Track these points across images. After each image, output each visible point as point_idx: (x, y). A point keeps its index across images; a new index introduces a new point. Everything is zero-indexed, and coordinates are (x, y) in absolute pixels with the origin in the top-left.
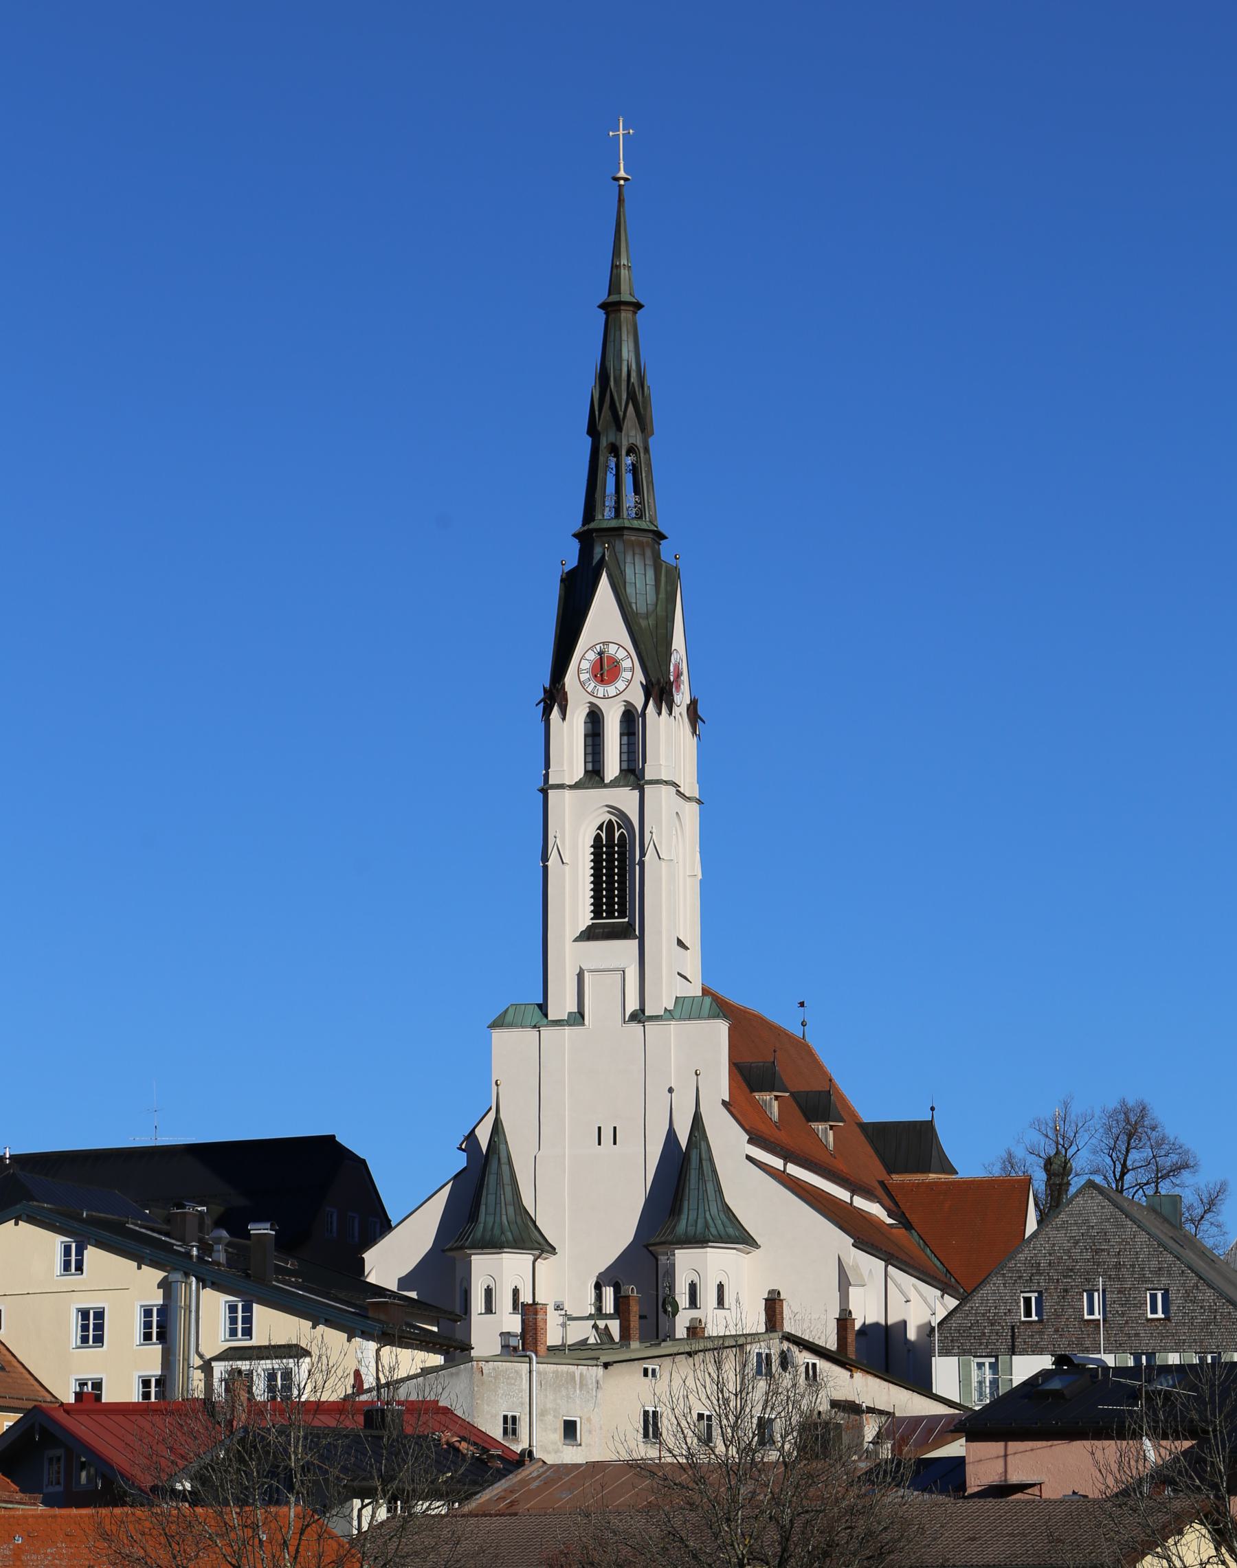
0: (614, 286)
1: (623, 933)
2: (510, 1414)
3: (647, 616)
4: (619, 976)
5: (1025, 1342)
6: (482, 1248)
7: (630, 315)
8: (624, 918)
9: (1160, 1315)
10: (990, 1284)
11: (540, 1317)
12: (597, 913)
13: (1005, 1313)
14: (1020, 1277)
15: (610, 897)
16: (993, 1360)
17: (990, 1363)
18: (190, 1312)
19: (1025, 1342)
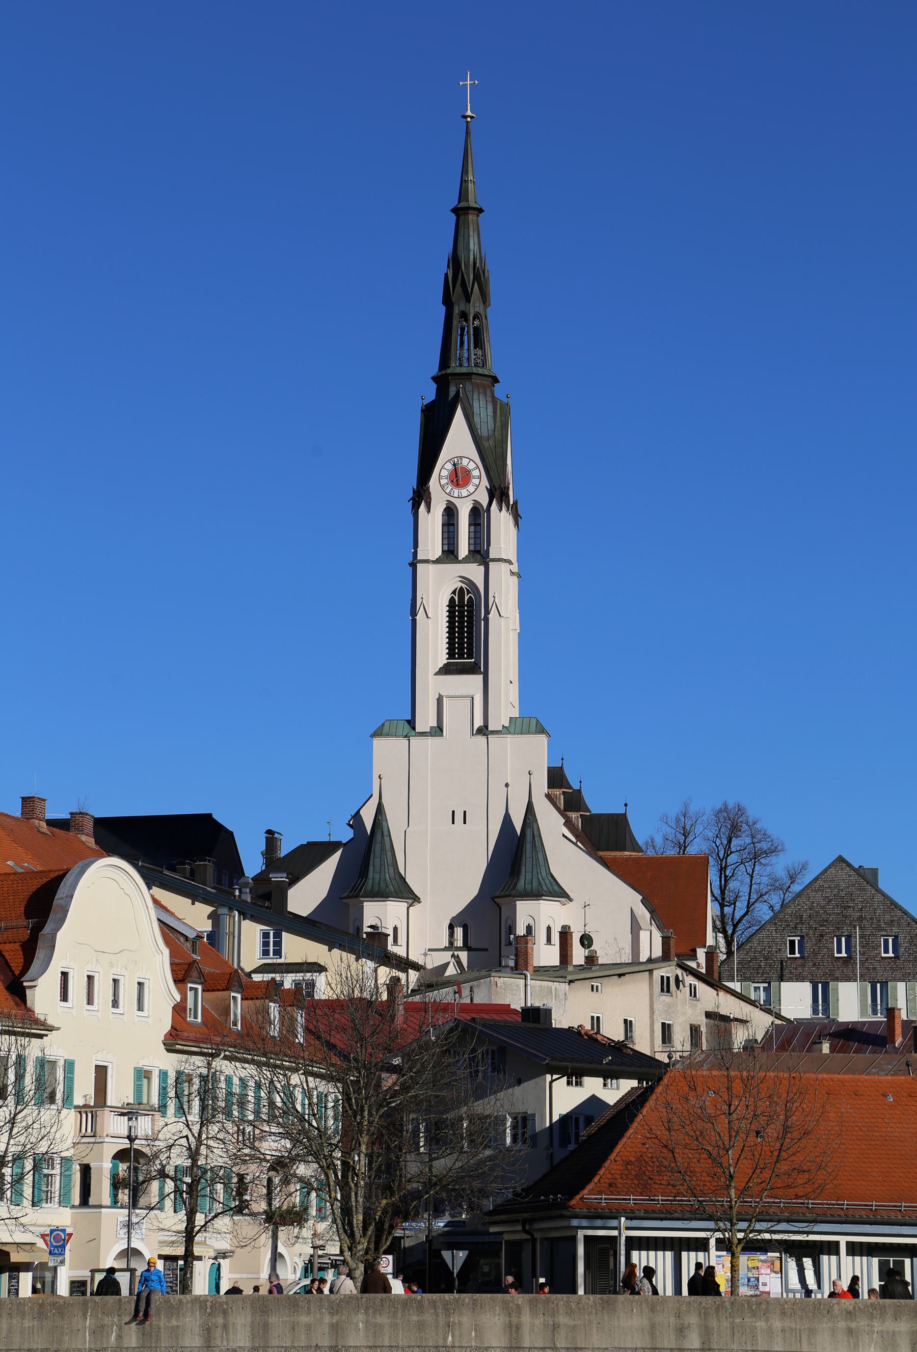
0: (463, 194)
1: (472, 670)
2: (595, 1015)
3: (488, 439)
4: (468, 701)
5: (791, 972)
6: (373, 897)
7: (475, 217)
8: (472, 659)
9: (891, 954)
10: (765, 930)
11: (529, 945)
12: (451, 655)
13: (776, 951)
14: (788, 926)
15: (461, 644)
16: (766, 985)
17: (764, 987)
18: (234, 937)
19: (791, 972)
